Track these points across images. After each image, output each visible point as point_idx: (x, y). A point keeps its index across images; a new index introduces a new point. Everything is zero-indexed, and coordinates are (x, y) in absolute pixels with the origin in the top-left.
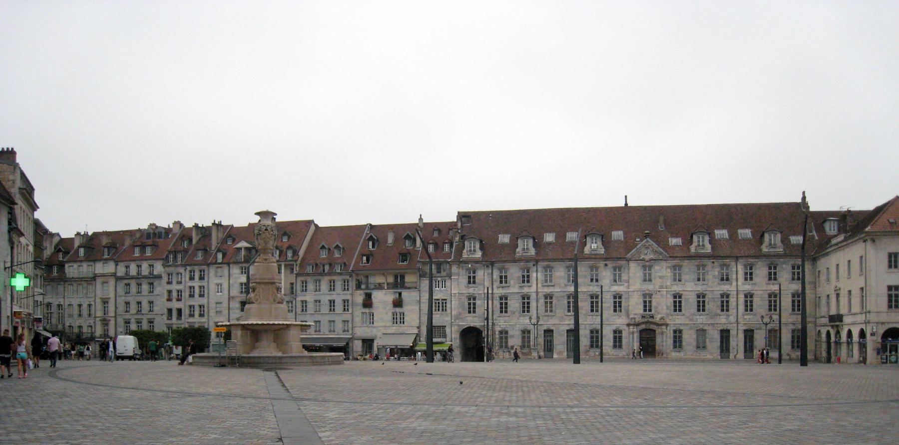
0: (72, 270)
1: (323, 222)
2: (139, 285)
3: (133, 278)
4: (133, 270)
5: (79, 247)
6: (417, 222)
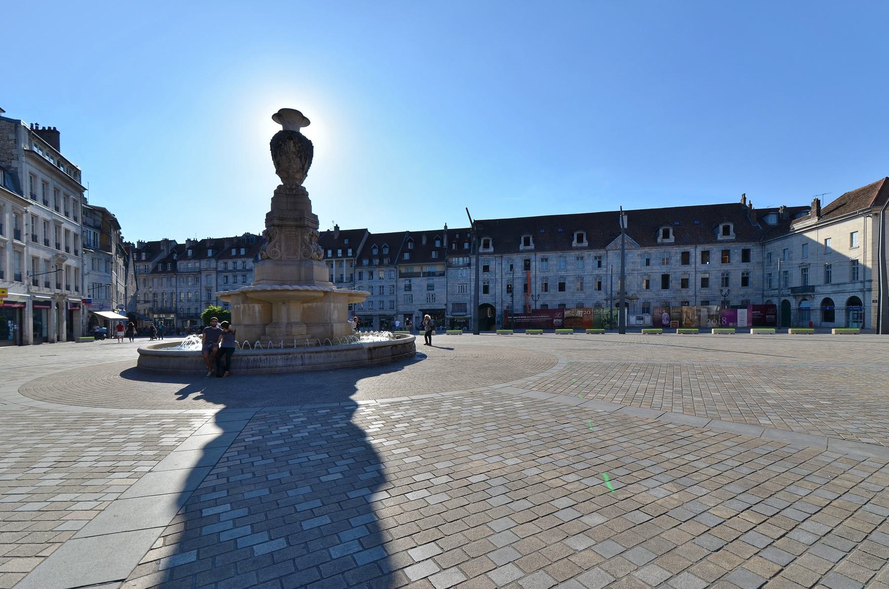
0: (182, 265)
1: (373, 231)
2: (235, 276)
3: (230, 271)
4: (230, 266)
5: (188, 249)
6: (443, 229)
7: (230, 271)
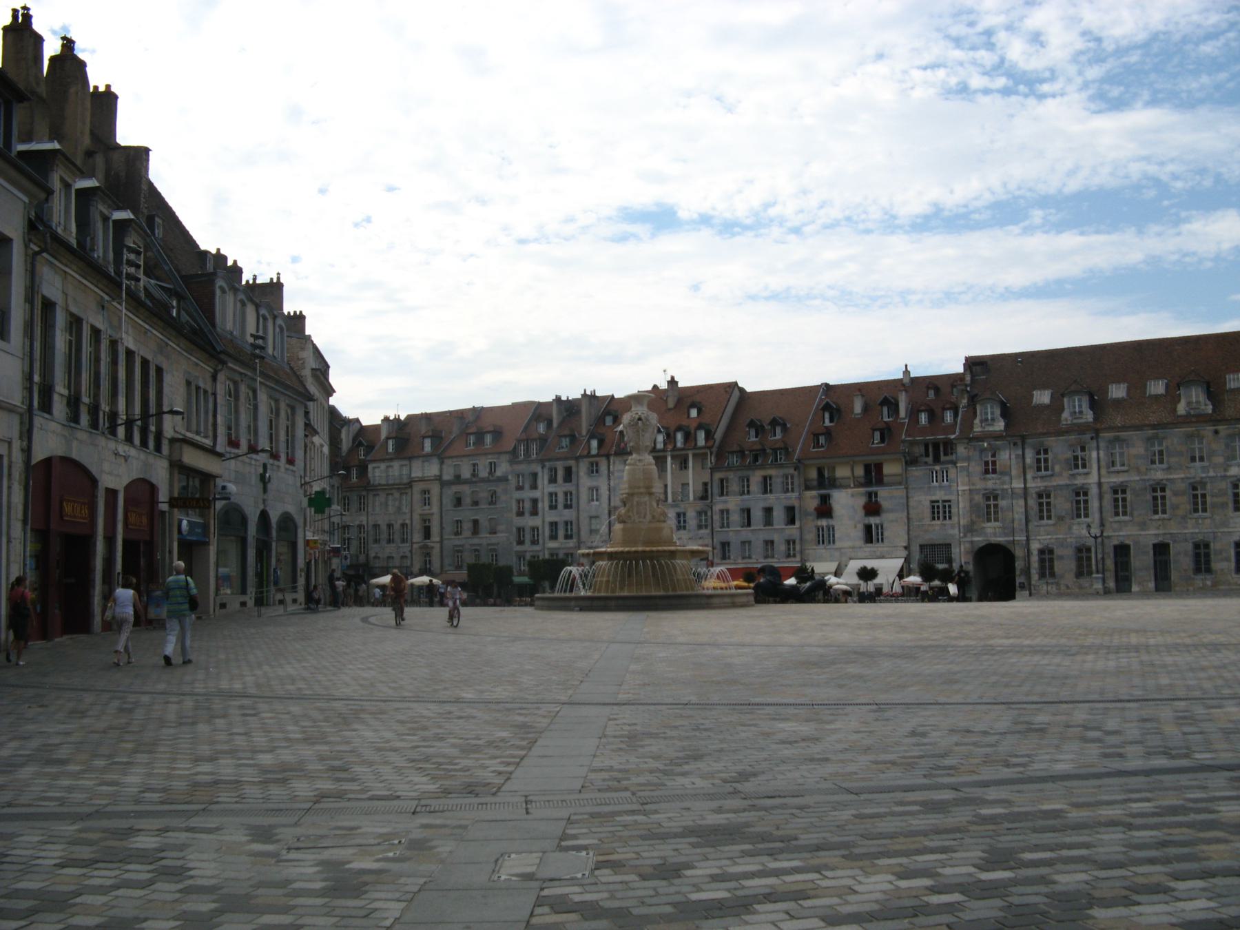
7: (466, 482)
